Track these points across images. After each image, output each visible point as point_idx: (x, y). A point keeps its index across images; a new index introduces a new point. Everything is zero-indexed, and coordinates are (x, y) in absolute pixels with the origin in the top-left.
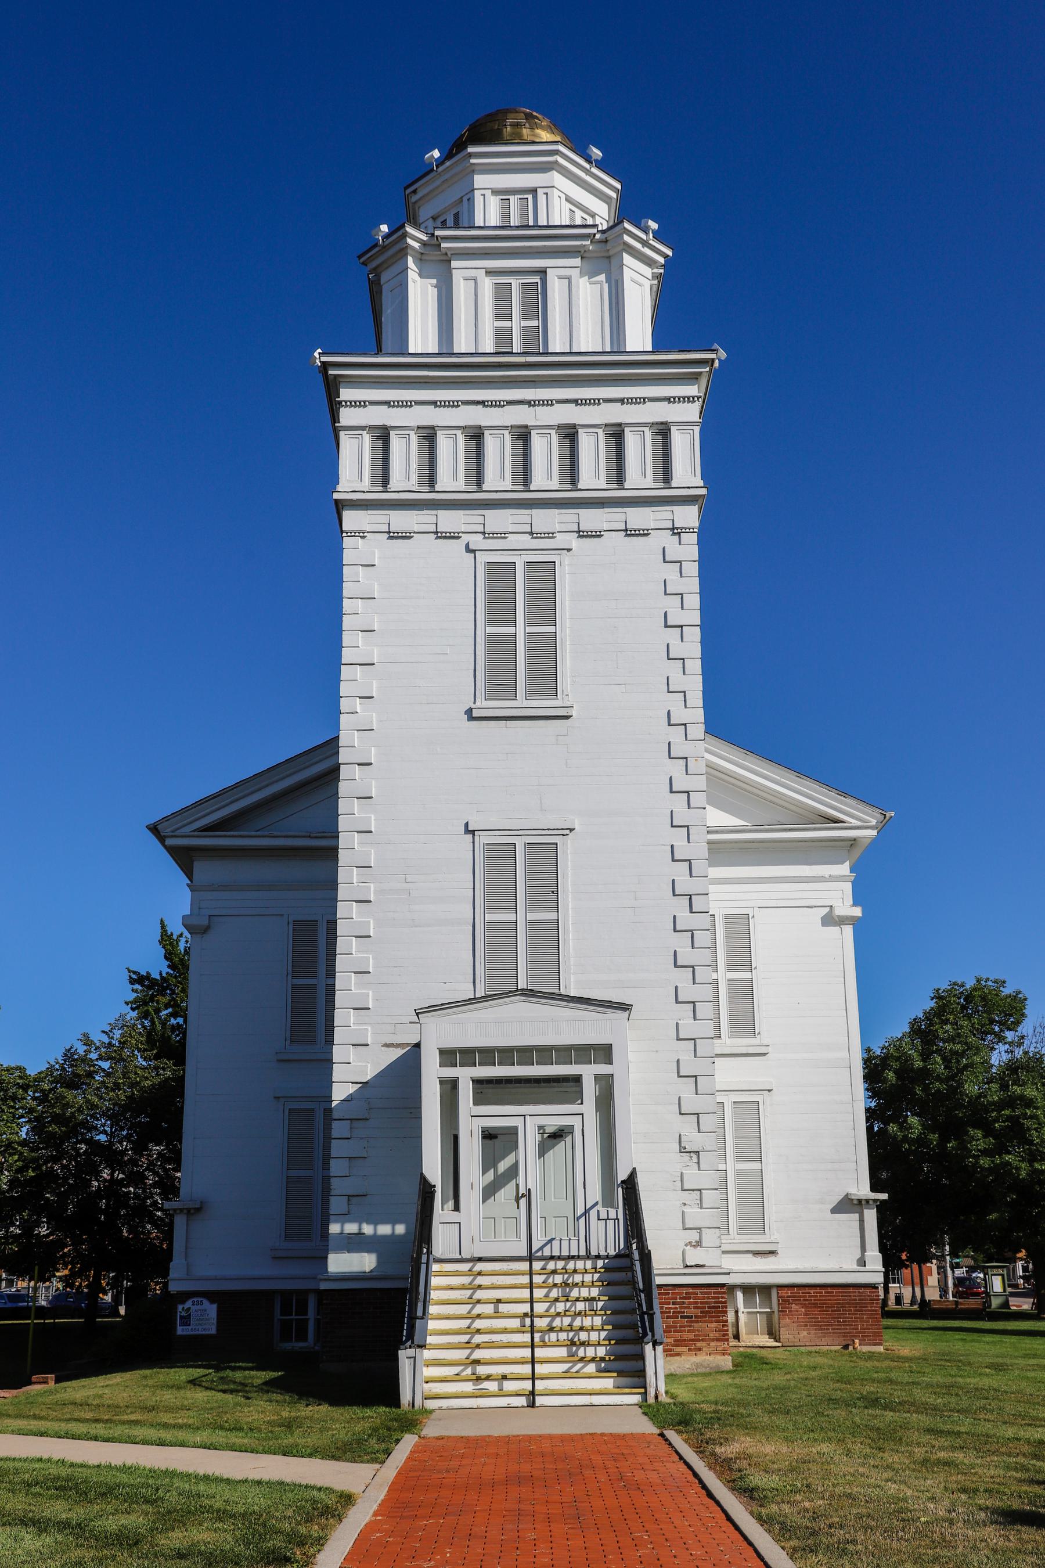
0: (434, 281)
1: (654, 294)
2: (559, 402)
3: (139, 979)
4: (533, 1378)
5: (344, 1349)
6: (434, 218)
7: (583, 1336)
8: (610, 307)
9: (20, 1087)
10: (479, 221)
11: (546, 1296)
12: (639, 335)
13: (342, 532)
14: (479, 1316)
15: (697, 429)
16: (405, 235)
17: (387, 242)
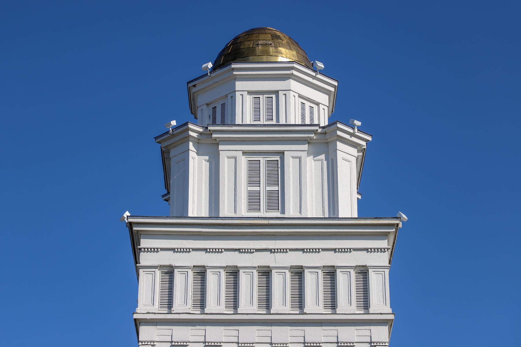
1: (359, 164)
2: (163, 249)
6: (207, 105)
8: (326, 183)
10: (238, 121)
12: (348, 207)
13: (139, 342)
15: (387, 271)
16: (188, 129)
17: (175, 133)
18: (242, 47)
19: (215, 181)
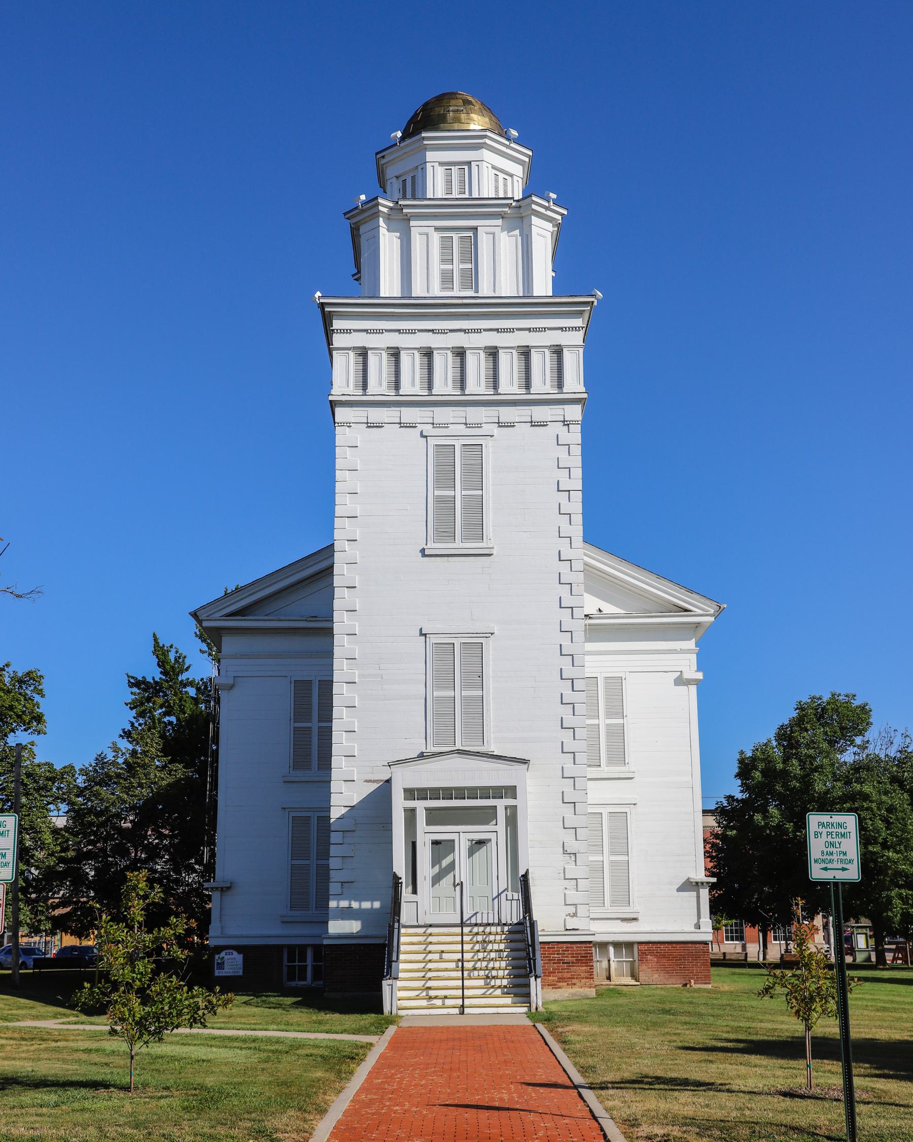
0: (398, 234)
3: (136, 683)
4: (463, 998)
5: (353, 978)
6: (397, 177)
7: (494, 973)
8: (520, 259)
9: (48, 779)
10: (430, 195)
11: (472, 949)
14: (430, 961)
15: (581, 350)
16: (378, 204)
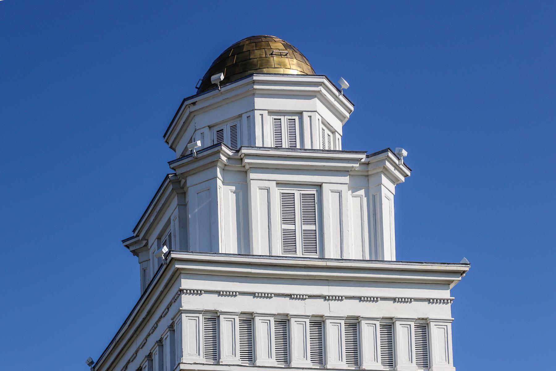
0: (234, 188)
2: (348, 298)
6: (210, 127)
8: (354, 221)
15: (449, 325)
16: (218, 152)
18: (252, 57)
19: (247, 214)
